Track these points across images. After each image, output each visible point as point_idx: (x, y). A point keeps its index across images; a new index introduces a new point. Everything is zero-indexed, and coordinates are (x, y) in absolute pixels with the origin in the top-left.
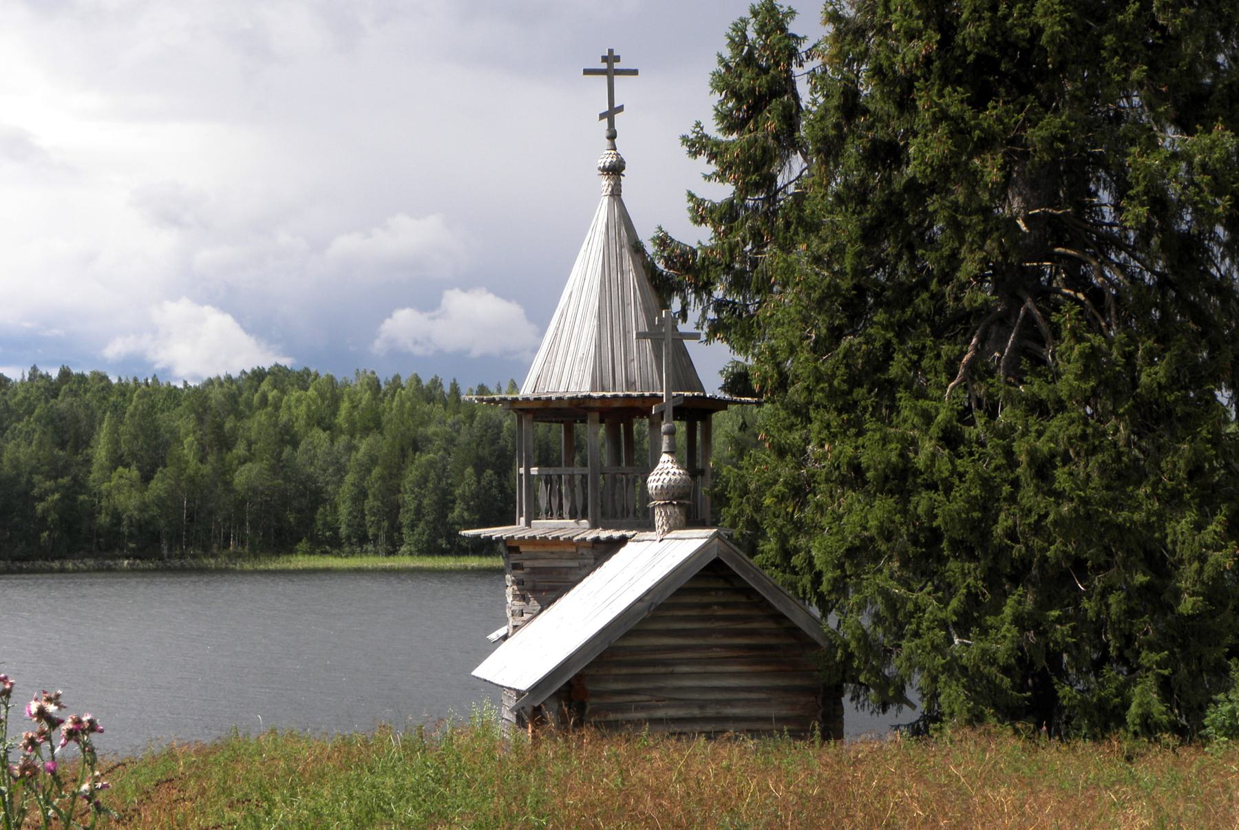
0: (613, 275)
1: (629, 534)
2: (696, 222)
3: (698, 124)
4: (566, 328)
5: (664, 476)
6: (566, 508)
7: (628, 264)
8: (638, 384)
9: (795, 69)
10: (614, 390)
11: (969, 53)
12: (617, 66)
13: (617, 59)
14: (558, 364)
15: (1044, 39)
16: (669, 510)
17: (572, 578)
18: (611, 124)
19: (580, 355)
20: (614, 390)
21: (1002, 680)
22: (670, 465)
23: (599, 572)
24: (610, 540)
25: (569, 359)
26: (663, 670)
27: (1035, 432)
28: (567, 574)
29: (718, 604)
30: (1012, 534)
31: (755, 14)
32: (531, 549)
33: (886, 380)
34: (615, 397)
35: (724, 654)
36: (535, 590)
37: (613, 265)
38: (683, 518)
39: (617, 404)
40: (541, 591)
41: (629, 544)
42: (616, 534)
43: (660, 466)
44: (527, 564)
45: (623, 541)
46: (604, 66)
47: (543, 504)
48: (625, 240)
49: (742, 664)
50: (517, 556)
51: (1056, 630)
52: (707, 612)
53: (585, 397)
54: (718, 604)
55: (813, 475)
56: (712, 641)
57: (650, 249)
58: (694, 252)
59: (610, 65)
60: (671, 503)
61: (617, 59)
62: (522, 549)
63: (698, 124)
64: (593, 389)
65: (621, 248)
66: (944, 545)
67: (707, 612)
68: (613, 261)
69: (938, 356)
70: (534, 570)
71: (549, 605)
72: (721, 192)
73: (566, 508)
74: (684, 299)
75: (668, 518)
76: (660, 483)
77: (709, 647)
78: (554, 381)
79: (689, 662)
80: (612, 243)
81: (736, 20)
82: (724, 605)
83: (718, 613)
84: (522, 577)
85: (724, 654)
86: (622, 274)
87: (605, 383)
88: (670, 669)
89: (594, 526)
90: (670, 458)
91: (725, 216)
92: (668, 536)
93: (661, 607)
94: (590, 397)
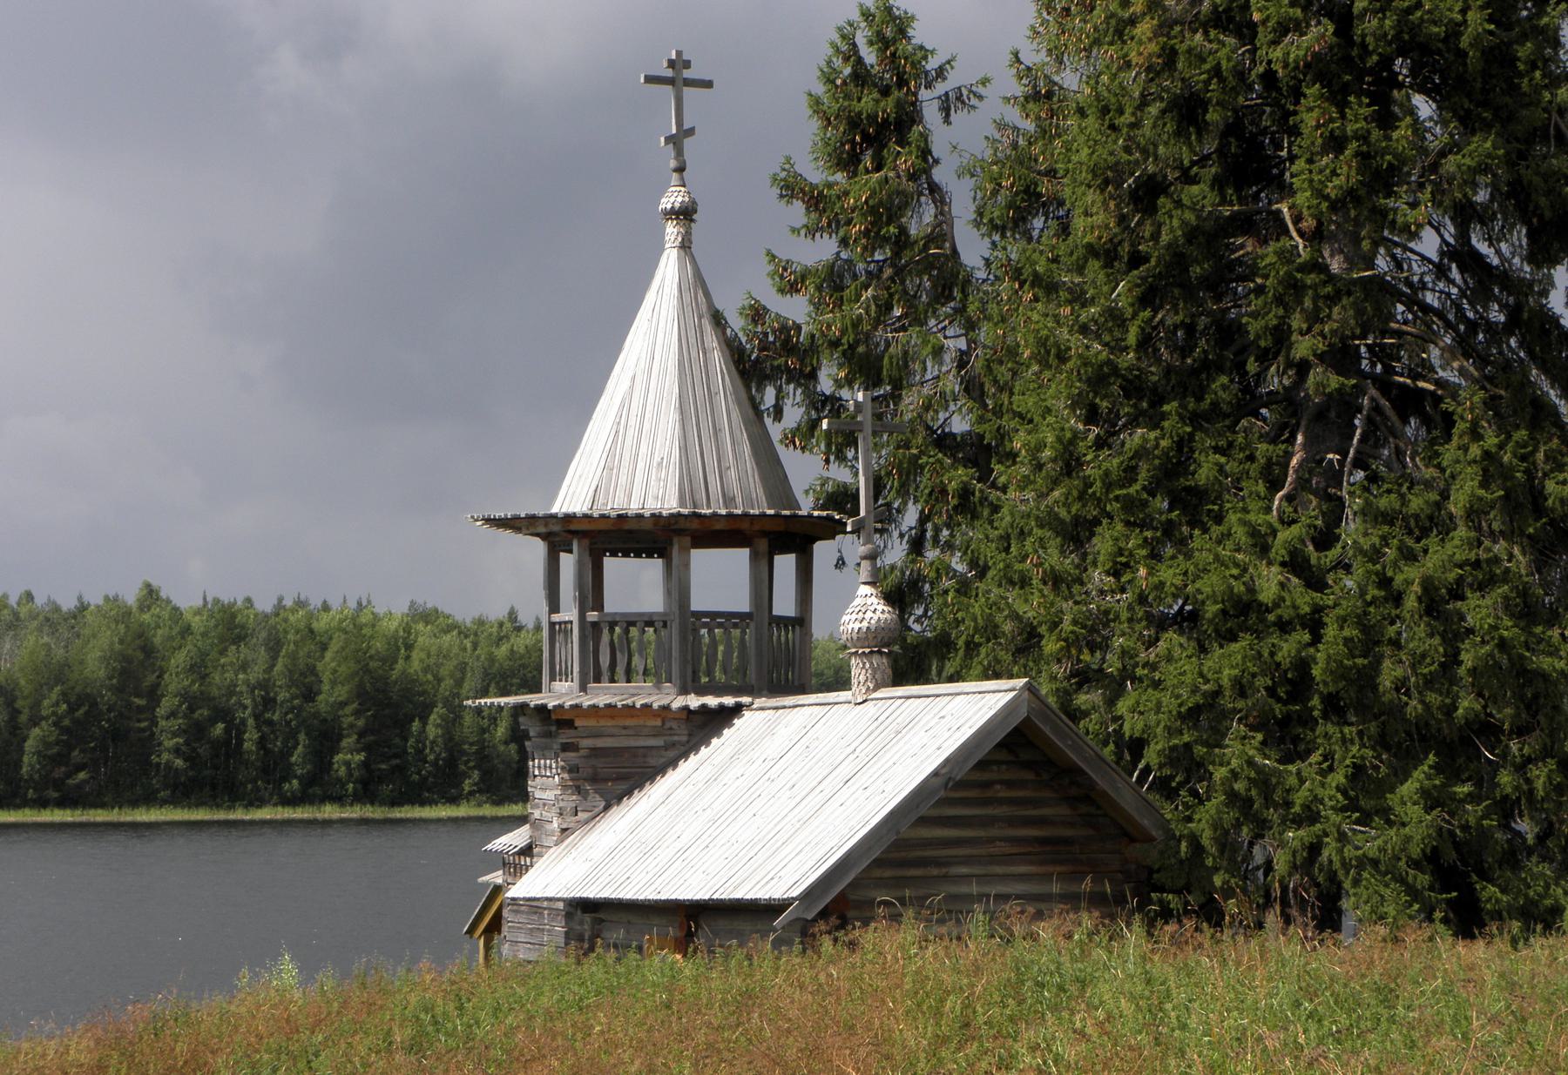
0: (694, 354)
1: (745, 700)
2: (781, 291)
3: (788, 160)
4: (632, 422)
5: (869, 614)
6: (620, 670)
7: (712, 341)
8: (739, 500)
9: (924, 94)
10: (709, 507)
11: (1371, 54)
12: (687, 74)
13: (687, 64)
14: (624, 470)
15: (1464, 42)
16: (876, 660)
17: (652, 761)
18: (679, 153)
19: (657, 459)
20: (709, 507)
21: (1415, 878)
22: (874, 600)
23: (693, 760)
24: (722, 707)
25: (641, 465)
26: (935, 872)
27: (1399, 552)
28: (645, 756)
29: (1001, 782)
30: (1401, 685)
31: (867, 15)
32: (592, 723)
33: (1188, 489)
34: (715, 515)
35: (1008, 849)
36: (595, 779)
37: (692, 341)
38: (889, 671)
39: (719, 526)
40: (606, 780)
41: (747, 714)
42: (729, 701)
43: (857, 601)
44: (585, 743)
45: (737, 710)
46: (669, 73)
47: (605, 660)
48: (704, 308)
49: (1031, 863)
50: (572, 732)
51: (1465, 811)
52: (989, 794)
53: (672, 515)
54: (1001, 782)
55: (1107, 612)
56: (995, 832)
57: (737, 323)
58: (798, 328)
59: (679, 72)
60: (880, 652)
61: (687, 64)
62: (577, 723)
63: (788, 160)
64: (682, 503)
65: (700, 318)
66: (1315, 701)
67: (989, 794)
68: (692, 333)
69: (1251, 458)
70: (595, 752)
71: (619, 800)
72: (821, 251)
73: (620, 670)
74: (779, 390)
75: (875, 671)
76: (865, 624)
77: (991, 841)
78: (620, 494)
79: (967, 861)
80: (688, 310)
81: (841, 23)
82: (1009, 784)
83: (1001, 794)
84: (577, 761)
85: (1008, 849)
86: (705, 353)
87: (697, 497)
88: (944, 870)
89: (684, 691)
90: (873, 591)
91: (833, 282)
92: (877, 695)
93: (961, 785)
94: (679, 515)
